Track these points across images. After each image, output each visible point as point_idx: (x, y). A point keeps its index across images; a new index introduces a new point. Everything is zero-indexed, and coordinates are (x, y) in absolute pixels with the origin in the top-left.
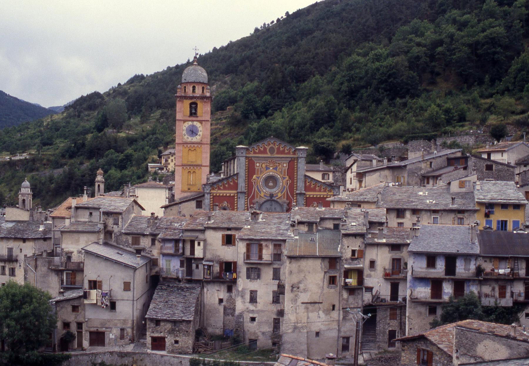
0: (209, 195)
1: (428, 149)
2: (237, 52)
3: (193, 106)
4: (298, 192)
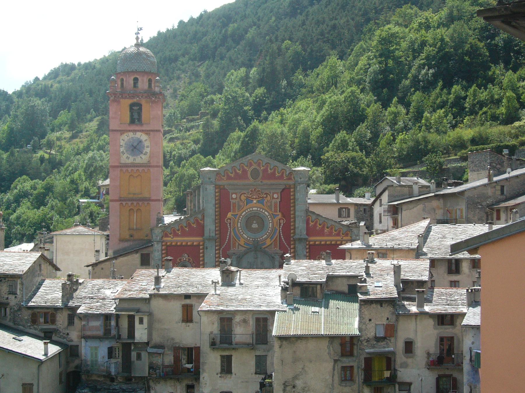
0: (160, 245)
1: (498, 166)
2: (214, 25)
3: (135, 108)
4: (297, 237)
